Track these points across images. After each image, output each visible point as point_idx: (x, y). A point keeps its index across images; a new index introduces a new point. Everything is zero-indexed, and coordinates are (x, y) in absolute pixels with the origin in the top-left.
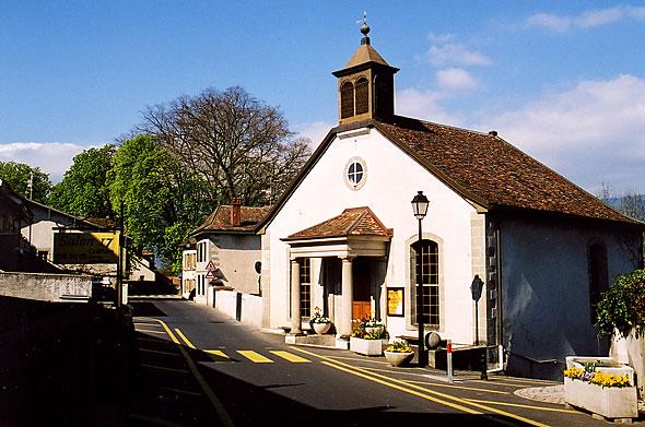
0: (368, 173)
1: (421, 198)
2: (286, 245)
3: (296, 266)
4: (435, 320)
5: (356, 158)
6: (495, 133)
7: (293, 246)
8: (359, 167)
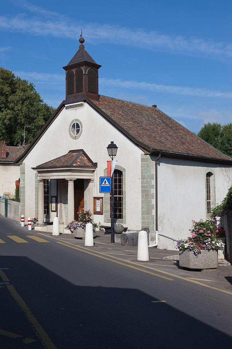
0: (84, 129)
1: (112, 147)
2: (35, 172)
3: (42, 184)
4: (121, 217)
5: (76, 120)
6: (155, 106)
7: (39, 172)
8: (78, 126)
